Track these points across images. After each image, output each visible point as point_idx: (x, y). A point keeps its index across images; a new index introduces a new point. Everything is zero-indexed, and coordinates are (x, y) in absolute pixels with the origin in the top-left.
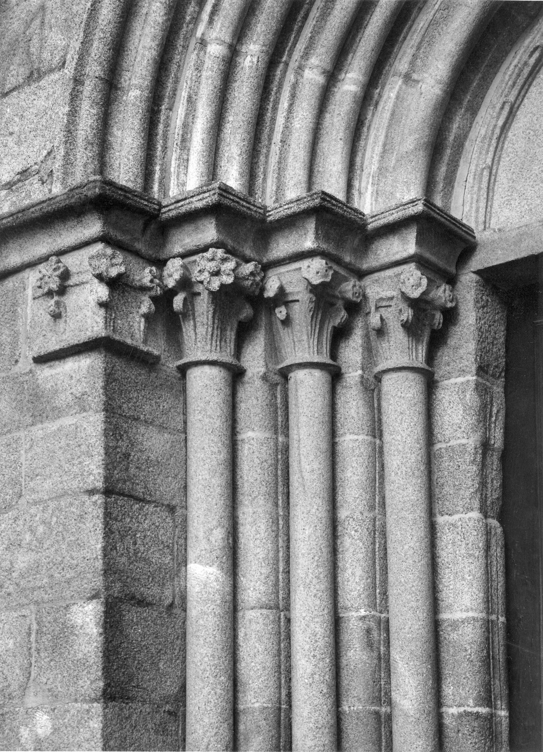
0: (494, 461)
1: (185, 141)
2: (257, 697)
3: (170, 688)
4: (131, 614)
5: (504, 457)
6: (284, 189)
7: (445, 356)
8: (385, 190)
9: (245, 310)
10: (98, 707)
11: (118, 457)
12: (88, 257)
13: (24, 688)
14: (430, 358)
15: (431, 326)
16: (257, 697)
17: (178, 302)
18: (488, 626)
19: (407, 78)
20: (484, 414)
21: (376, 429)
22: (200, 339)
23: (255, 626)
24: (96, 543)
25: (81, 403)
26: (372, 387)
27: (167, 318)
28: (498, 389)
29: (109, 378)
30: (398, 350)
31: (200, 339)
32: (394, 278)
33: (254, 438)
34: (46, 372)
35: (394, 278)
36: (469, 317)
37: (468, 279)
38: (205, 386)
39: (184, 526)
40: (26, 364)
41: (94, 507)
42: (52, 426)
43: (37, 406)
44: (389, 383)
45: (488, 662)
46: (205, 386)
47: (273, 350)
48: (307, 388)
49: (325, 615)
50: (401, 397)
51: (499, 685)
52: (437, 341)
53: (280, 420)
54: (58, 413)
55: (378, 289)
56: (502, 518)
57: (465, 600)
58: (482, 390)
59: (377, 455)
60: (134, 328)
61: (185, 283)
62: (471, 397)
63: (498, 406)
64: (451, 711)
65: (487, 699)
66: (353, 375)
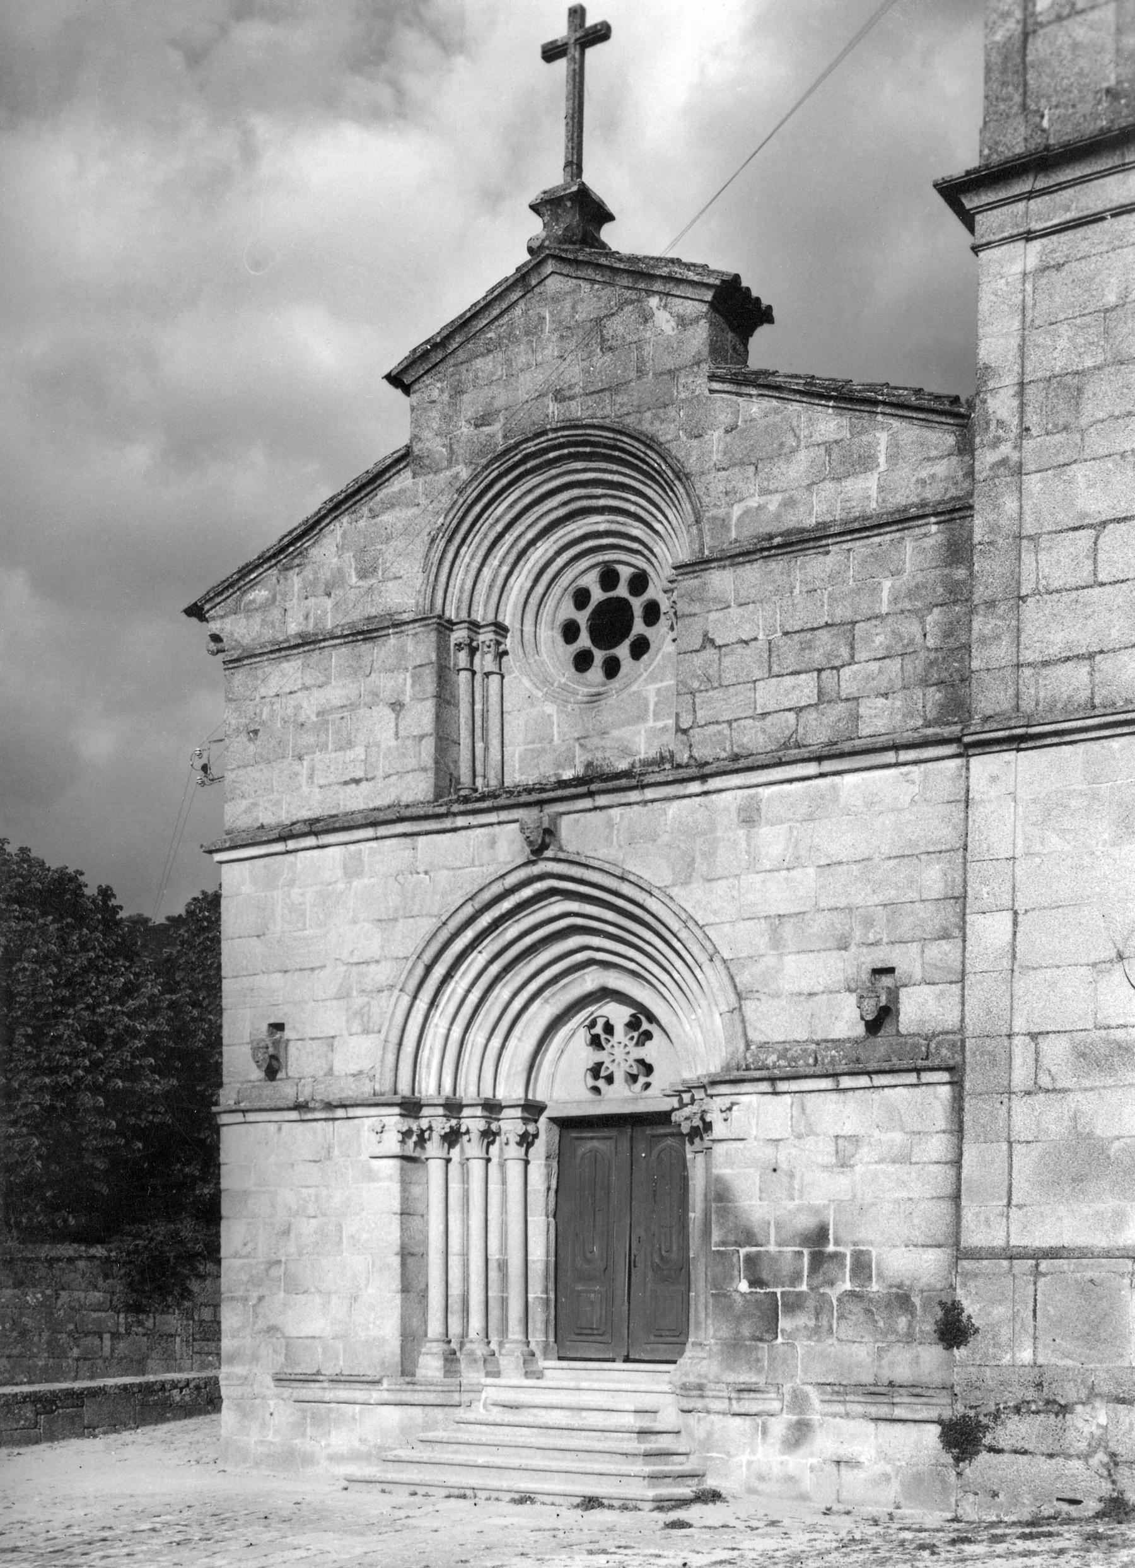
0: (552, 1193)
1: (428, 1066)
2: (455, 1290)
3: (422, 1286)
4: (410, 1260)
5: (557, 1191)
6: (468, 1092)
7: (532, 1150)
8: (510, 1090)
9: (452, 1138)
10: (399, 1296)
11: (405, 1199)
12: (393, 1120)
13: (367, 1286)
14: (526, 1154)
15: (526, 1140)
16: (455, 1290)
17: (426, 1135)
18: (547, 1263)
19: (519, 1039)
20: (549, 1176)
21: (504, 1182)
22: (434, 1148)
23: (455, 1262)
24: (398, 1234)
25: (390, 1178)
26: (502, 1165)
27: (422, 1141)
28: (555, 1164)
29: (402, 1169)
30: (514, 1151)
31: (434, 1148)
32: (511, 1125)
33: (455, 1187)
34: (374, 1162)
35: (511, 1125)
36: (543, 1136)
37: (543, 1120)
38: (435, 1167)
39: (427, 1223)
40: (364, 1157)
41: (396, 1220)
42: (377, 1185)
43: (370, 1176)
44: (509, 1164)
45: (547, 1277)
46: (435, 1167)
47: (462, 1151)
48: (477, 1167)
49: (483, 1259)
50: (515, 1169)
51: (551, 1286)
52: (530, 1145)
53: (465, 1178)
54: (379, 1180)
55: (505, 1125)
56: (555, 1217)
57: (538, 1252)
58: (548, 1166)
59: (504, 1193)
60: (410, 1148)
61: (430, 1128)
62: (543, 1170)
63: (555, 1170)
64: (531, 1296)
65: (546, 1291)
66: (495, 1161)
